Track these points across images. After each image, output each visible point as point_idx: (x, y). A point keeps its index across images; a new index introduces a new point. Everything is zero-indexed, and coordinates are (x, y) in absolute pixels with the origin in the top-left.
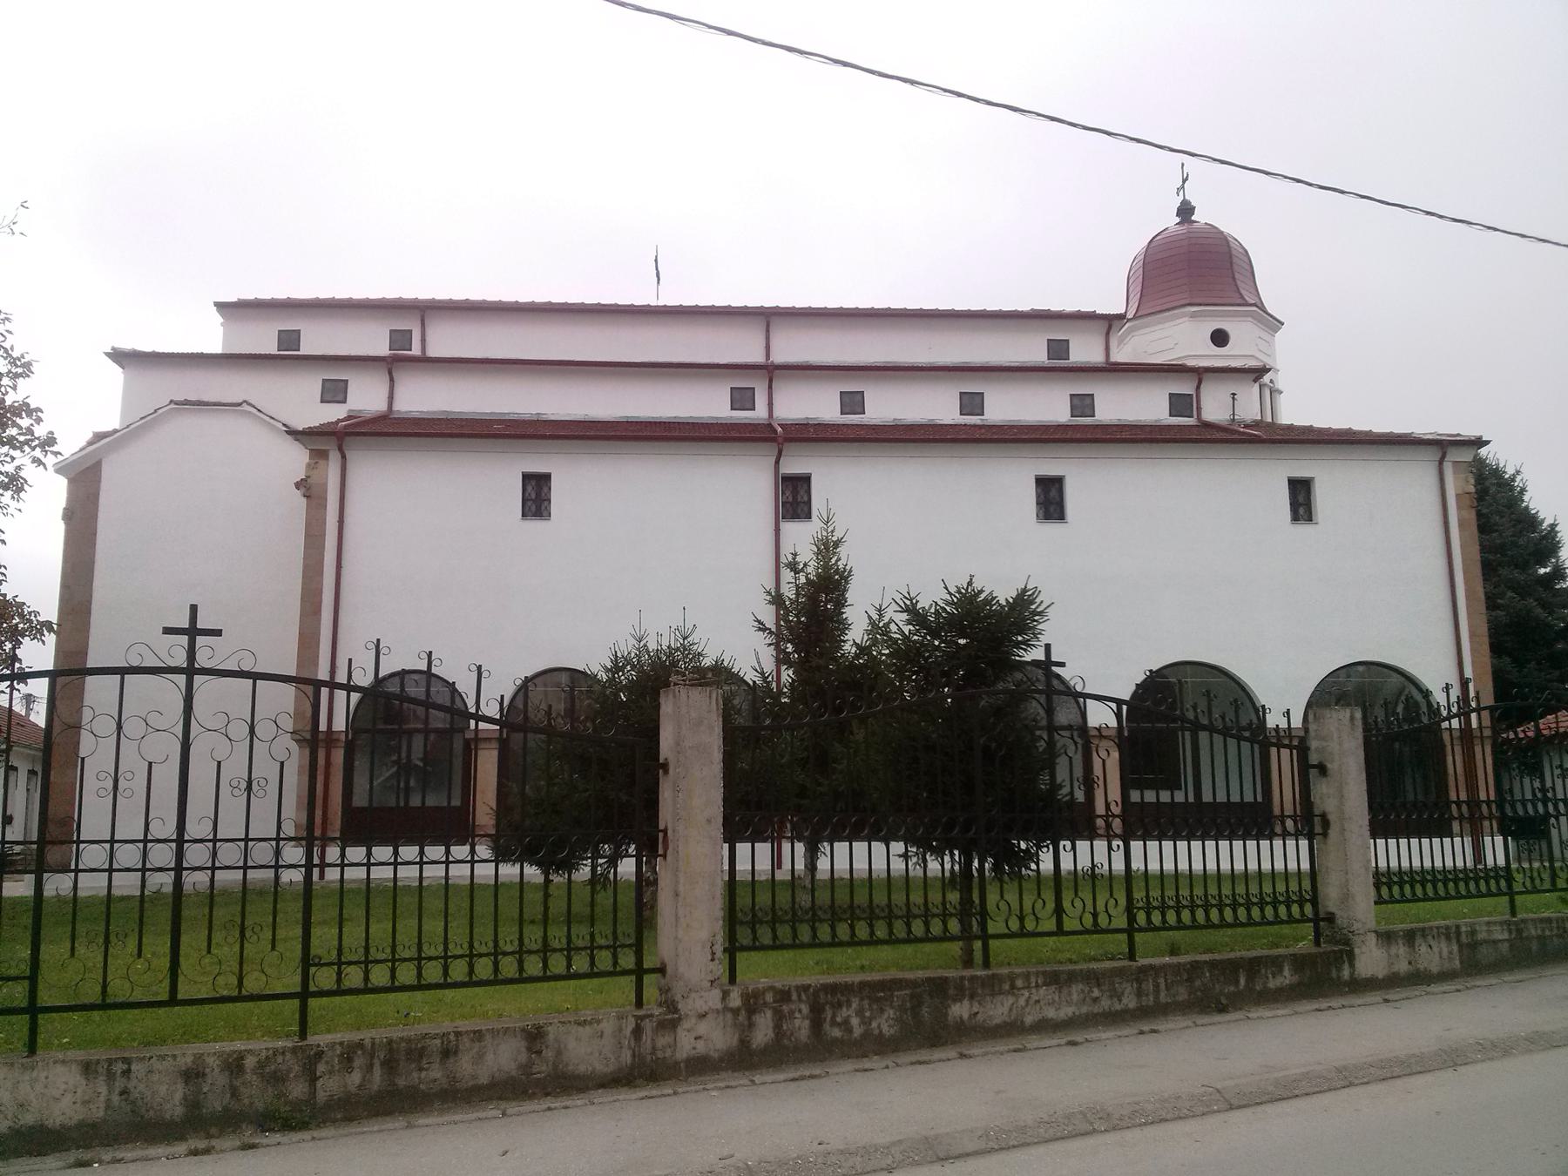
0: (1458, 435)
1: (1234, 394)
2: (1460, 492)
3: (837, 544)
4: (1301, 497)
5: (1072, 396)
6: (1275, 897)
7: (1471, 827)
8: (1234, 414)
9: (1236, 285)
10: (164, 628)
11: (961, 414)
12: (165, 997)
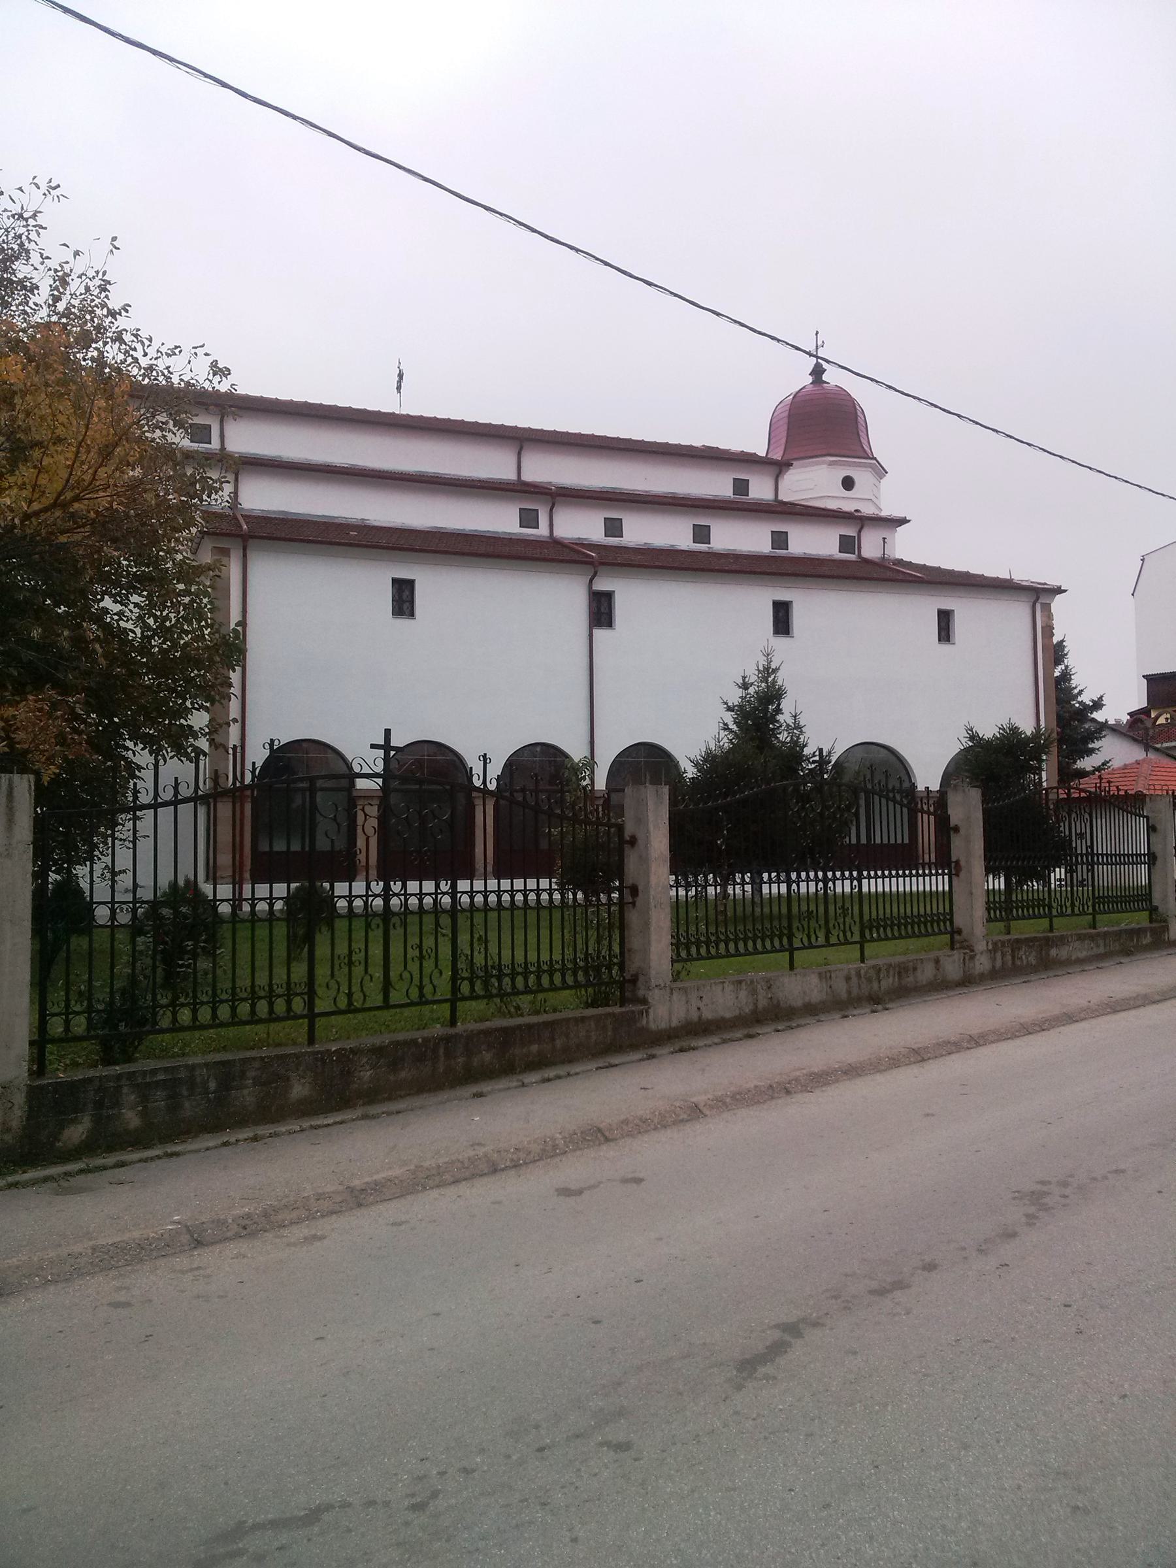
0: (1045, 584)
1: (884, 538)
2: (1044, 625)
3: (775, 671)
4: (945, 624)
5: (772, 532)
6: (539, 966)
7: (288, 927)
8: (884, 554)
9: (860, 441)
10: (390, 730)
11: (694, 542)
12: (379, 1003)
